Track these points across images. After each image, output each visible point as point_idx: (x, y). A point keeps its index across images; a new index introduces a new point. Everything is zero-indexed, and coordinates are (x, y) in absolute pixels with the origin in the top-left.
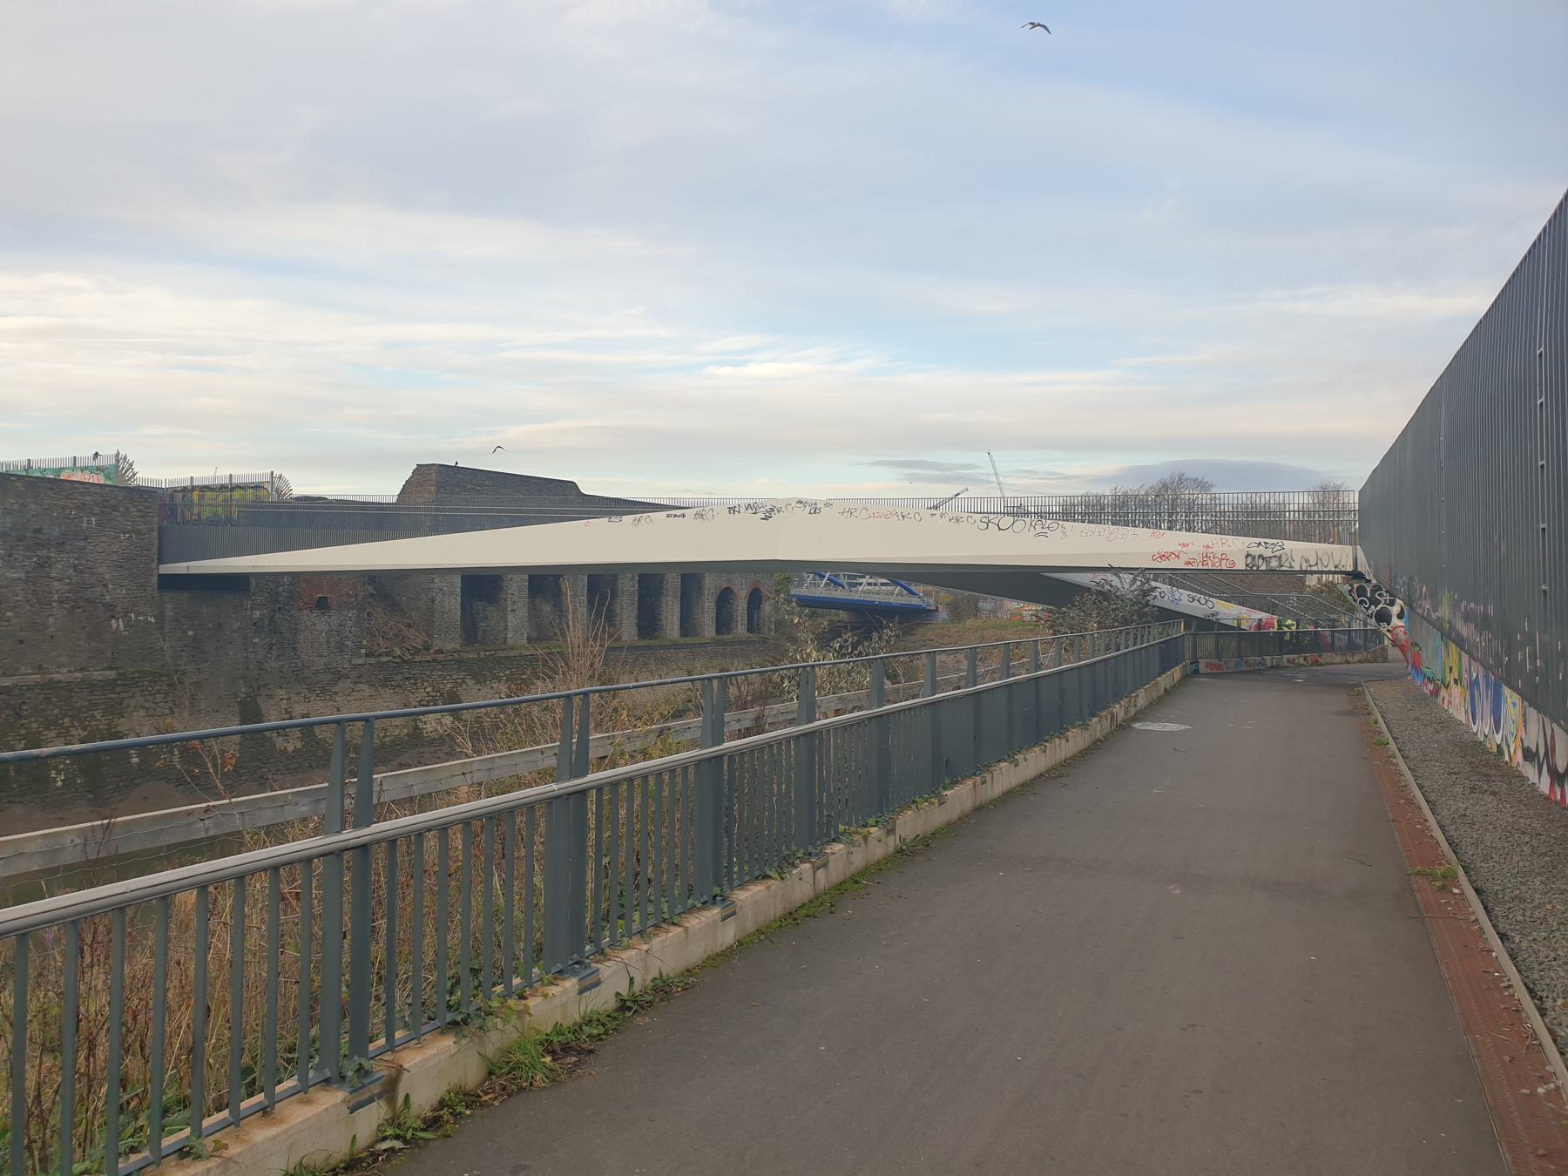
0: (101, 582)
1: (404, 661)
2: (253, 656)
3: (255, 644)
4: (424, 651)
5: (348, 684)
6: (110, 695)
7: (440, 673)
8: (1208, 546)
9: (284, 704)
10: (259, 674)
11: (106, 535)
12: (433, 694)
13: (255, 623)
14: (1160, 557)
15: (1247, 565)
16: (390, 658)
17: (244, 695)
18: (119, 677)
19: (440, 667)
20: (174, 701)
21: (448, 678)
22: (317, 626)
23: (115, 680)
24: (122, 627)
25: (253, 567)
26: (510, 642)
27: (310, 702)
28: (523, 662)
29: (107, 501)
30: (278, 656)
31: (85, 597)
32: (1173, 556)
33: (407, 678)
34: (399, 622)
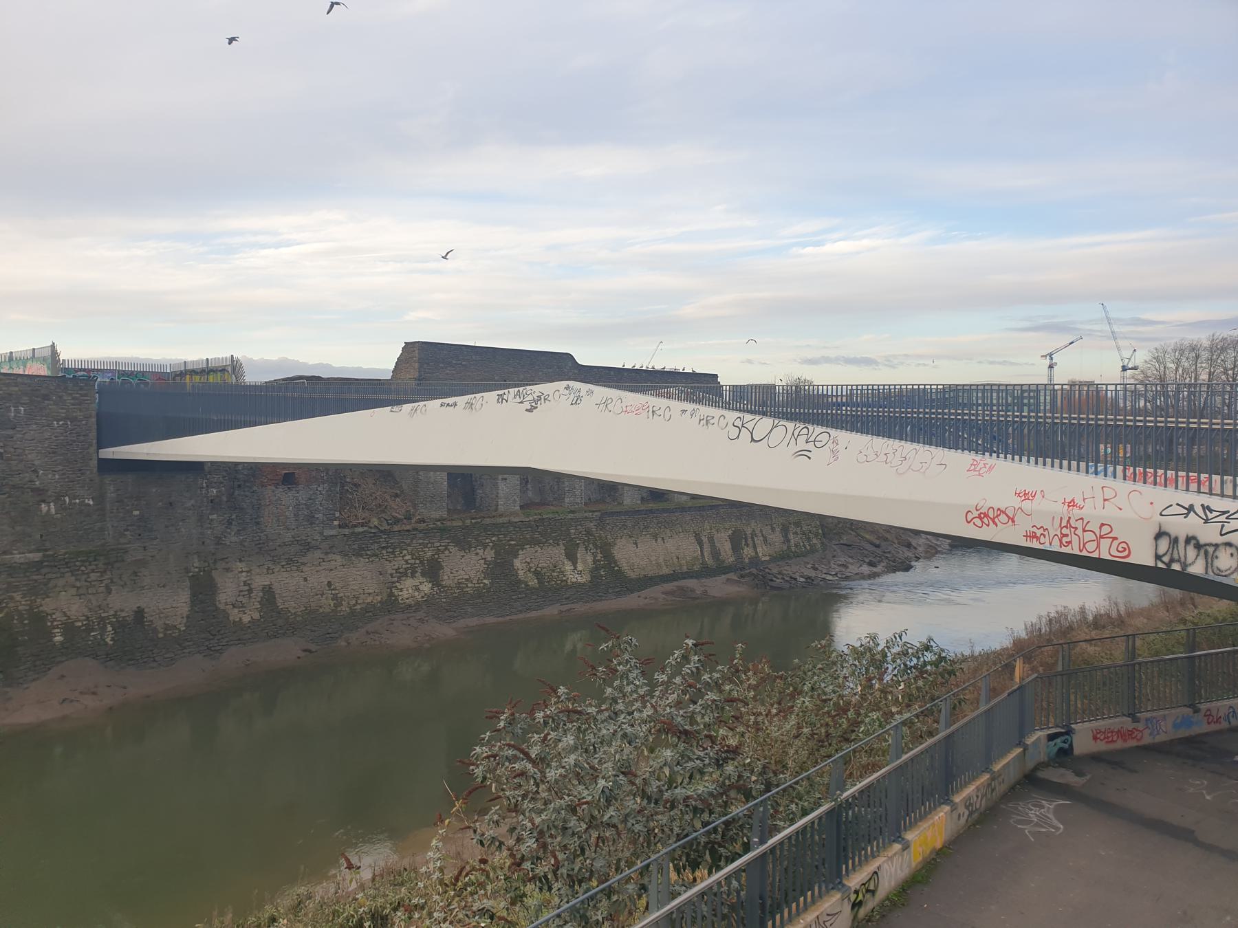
0: (30, 468)
1: (382, 532)
2: (209, 532)
3: (212, 520)
4: (405, 520)
5: (318, 554)
6: (35, 577)
7: (421, 541)
8: (1072, 504)
9: (243, 577)
10: (216, 549)
11: (36, 424)
12: (413, 561)
13: (212, 500)
14: (979, 517)
15: (1158, 557)
16: (365, 529)
17: (197, 570)
18: (45, 559)
19: (421, 535)
20: (111, 579)
21: (429, 545)
22: (288, 499)
23: (41, 562)
24: (53, 511)
25: (148, 454)
26: (501, 508)
27: (273, 573)
28: (512, 528)
29: (37, 390)
30: (238, 530)
31: (11, 483)
32: (1003, 518)
33: (383, 548)
34: (385, 493)
